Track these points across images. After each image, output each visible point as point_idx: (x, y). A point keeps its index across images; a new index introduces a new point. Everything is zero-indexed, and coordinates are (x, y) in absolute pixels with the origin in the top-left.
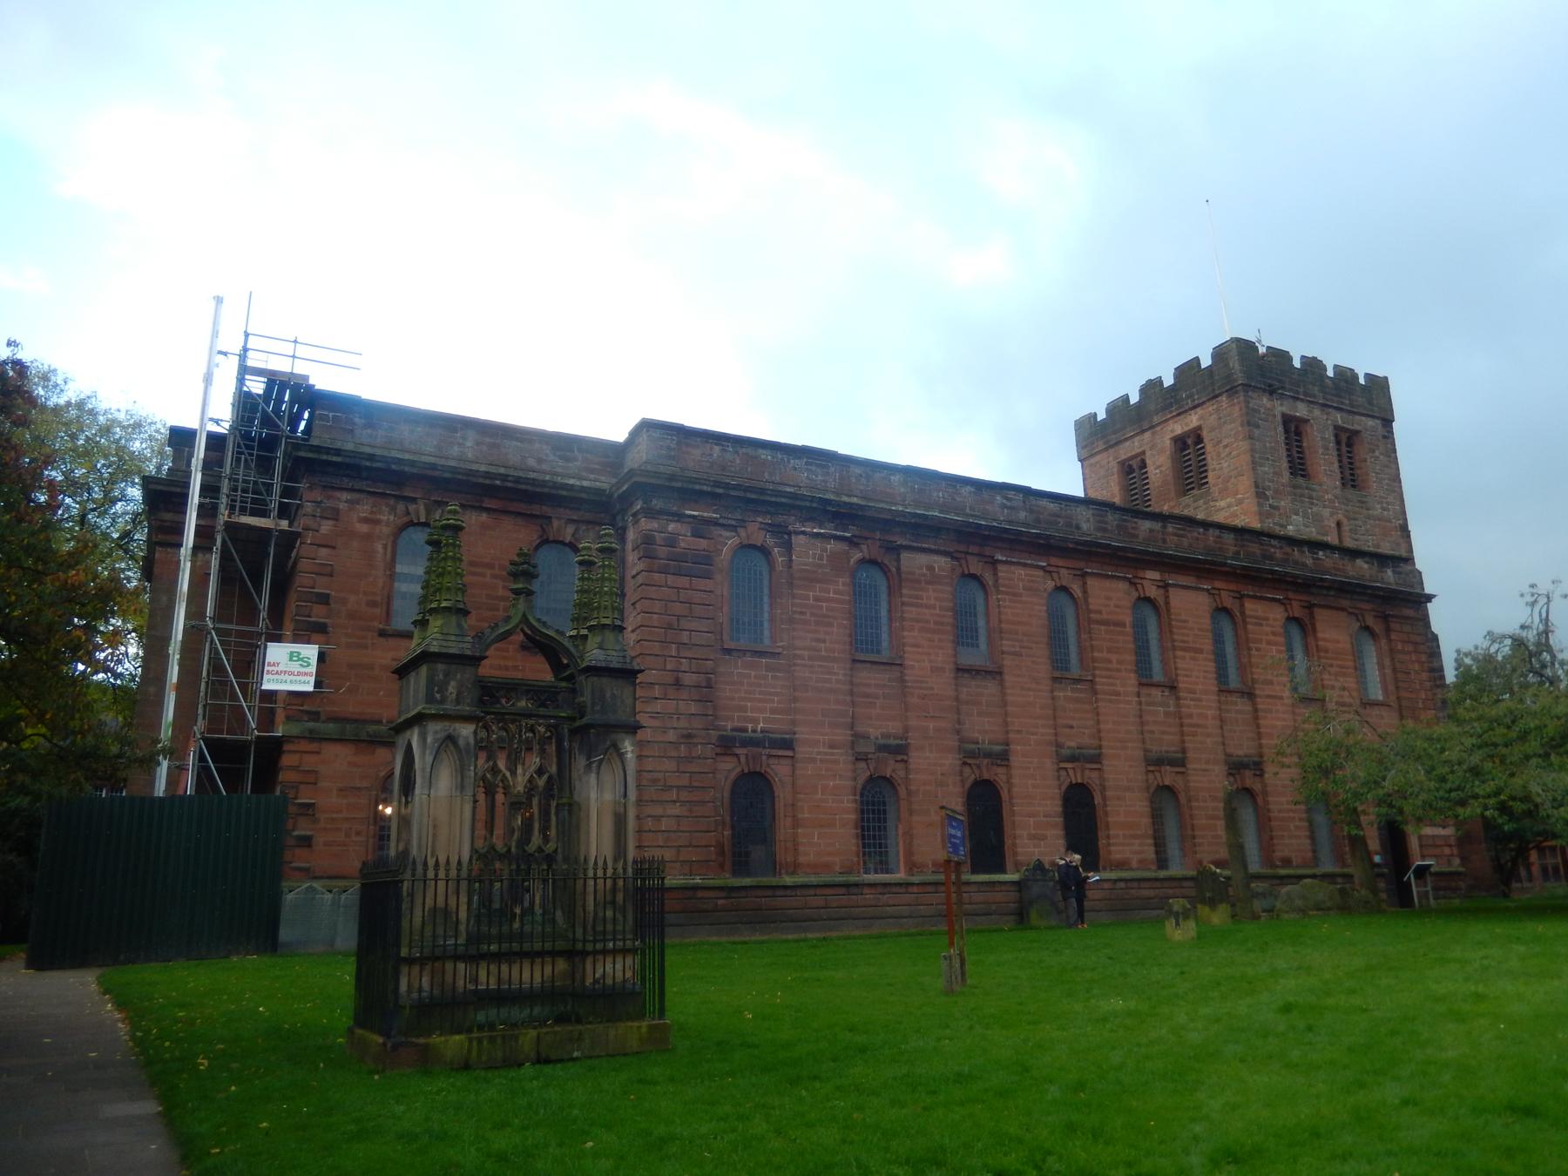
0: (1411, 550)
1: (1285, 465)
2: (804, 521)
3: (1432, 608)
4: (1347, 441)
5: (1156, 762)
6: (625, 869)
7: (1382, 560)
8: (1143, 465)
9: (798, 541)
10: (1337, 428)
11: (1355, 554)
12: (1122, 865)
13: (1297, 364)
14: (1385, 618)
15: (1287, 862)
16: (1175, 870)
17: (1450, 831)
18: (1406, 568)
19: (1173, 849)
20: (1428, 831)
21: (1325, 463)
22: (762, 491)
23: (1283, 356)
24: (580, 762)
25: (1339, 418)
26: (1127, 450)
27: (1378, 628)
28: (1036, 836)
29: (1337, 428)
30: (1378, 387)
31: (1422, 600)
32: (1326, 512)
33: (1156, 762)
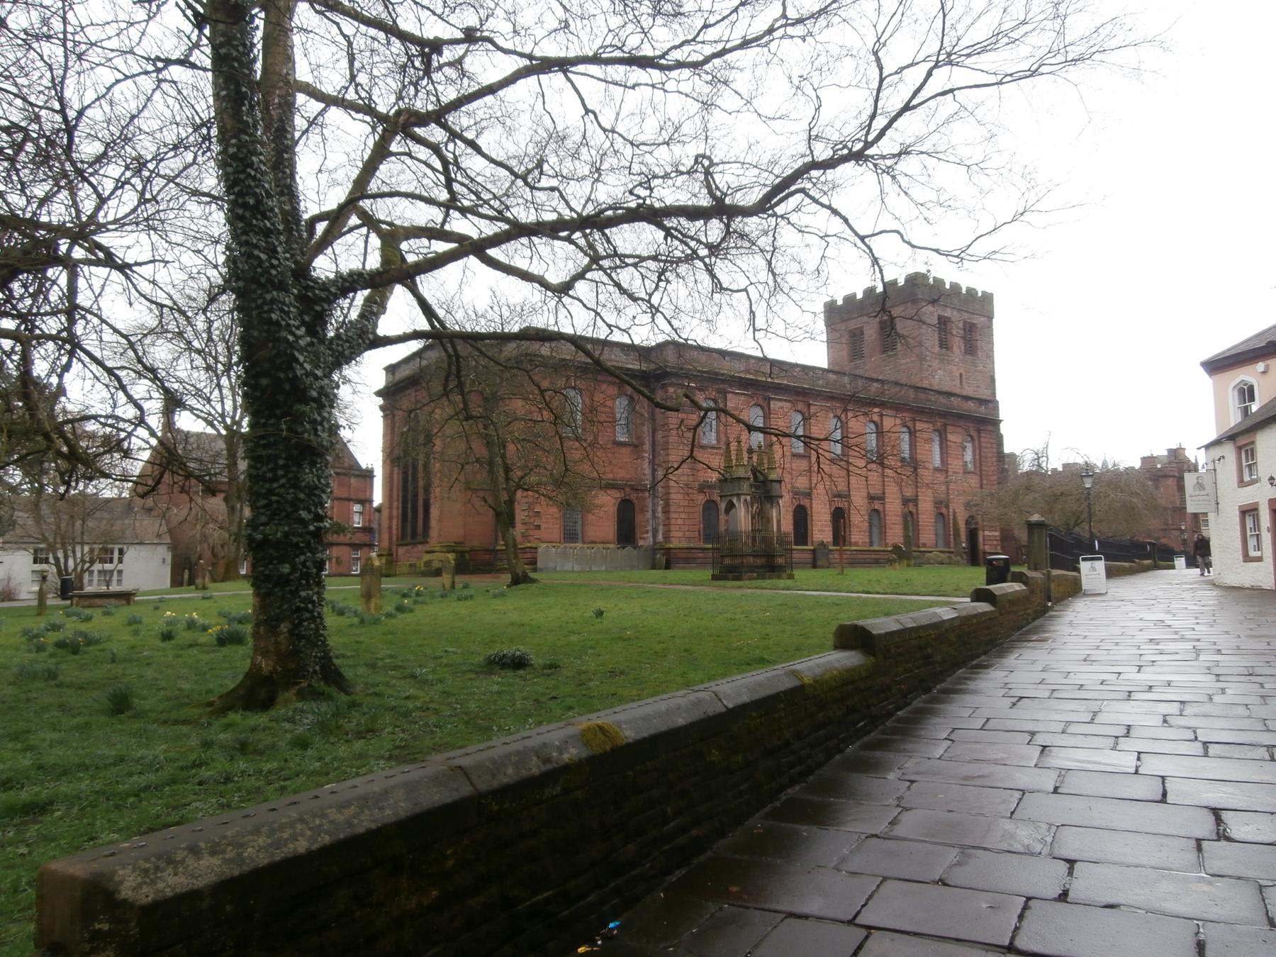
0: (994, 394)
1: (937, 343)
2: (731, 386)
3: (1002, 426)
4: (970, 329)
5: (871, 498)
6: (74, 552)
7: (982, 402)
8: (862, 333)
9: (729, 396)
10: (965, 322)
11: (967, 398)
12: (856, 544)
13: (948, 286)
14: (979, 431)
15: (924, 545)
16: (875, 548)
17: (997, 534)
18: (991, 405)
19: (876, 539)
20: (987, 533)
21: (957, 345)
22: (717, 374)
23: (942, 282)
24: (768, 506)
25: (966, 316)
26: (853, 325)
27: (974, 434)
28: (821, 530)
29: (965, 322)
30: (987, 299)
31: (996, 423)
32: (955, 368)
33: (871, 498)
